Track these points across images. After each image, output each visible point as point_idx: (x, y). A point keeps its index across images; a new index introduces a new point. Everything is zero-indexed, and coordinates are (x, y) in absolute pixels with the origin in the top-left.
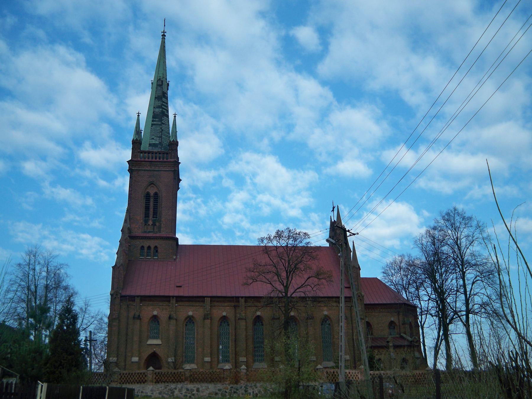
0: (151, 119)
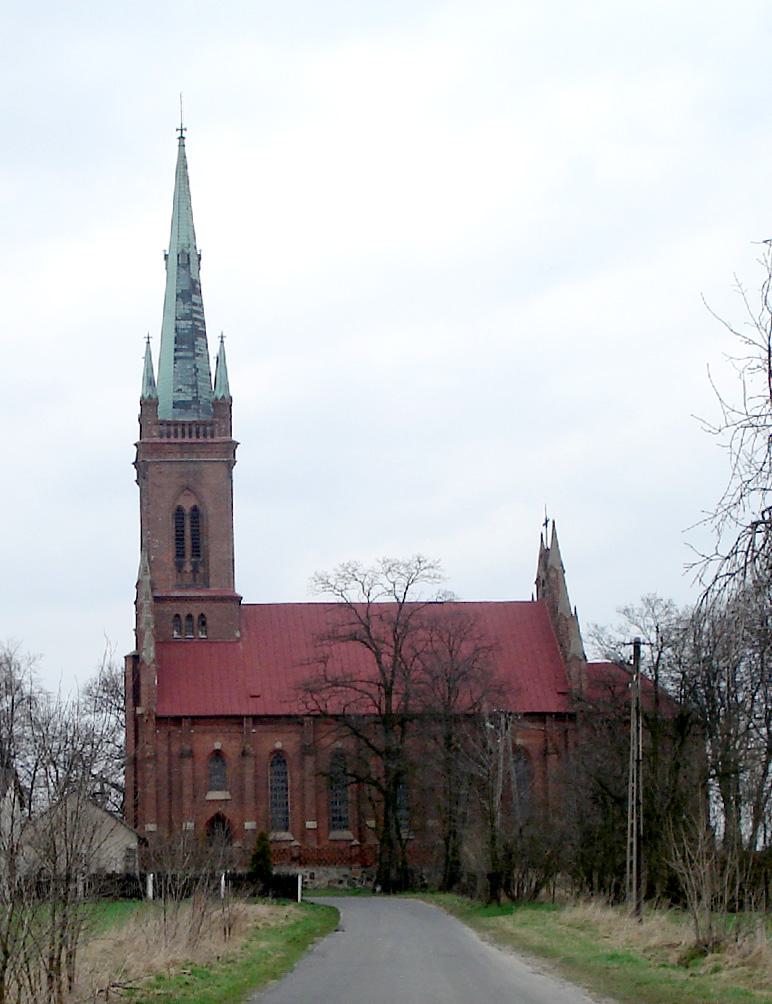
0: (173, 346)
